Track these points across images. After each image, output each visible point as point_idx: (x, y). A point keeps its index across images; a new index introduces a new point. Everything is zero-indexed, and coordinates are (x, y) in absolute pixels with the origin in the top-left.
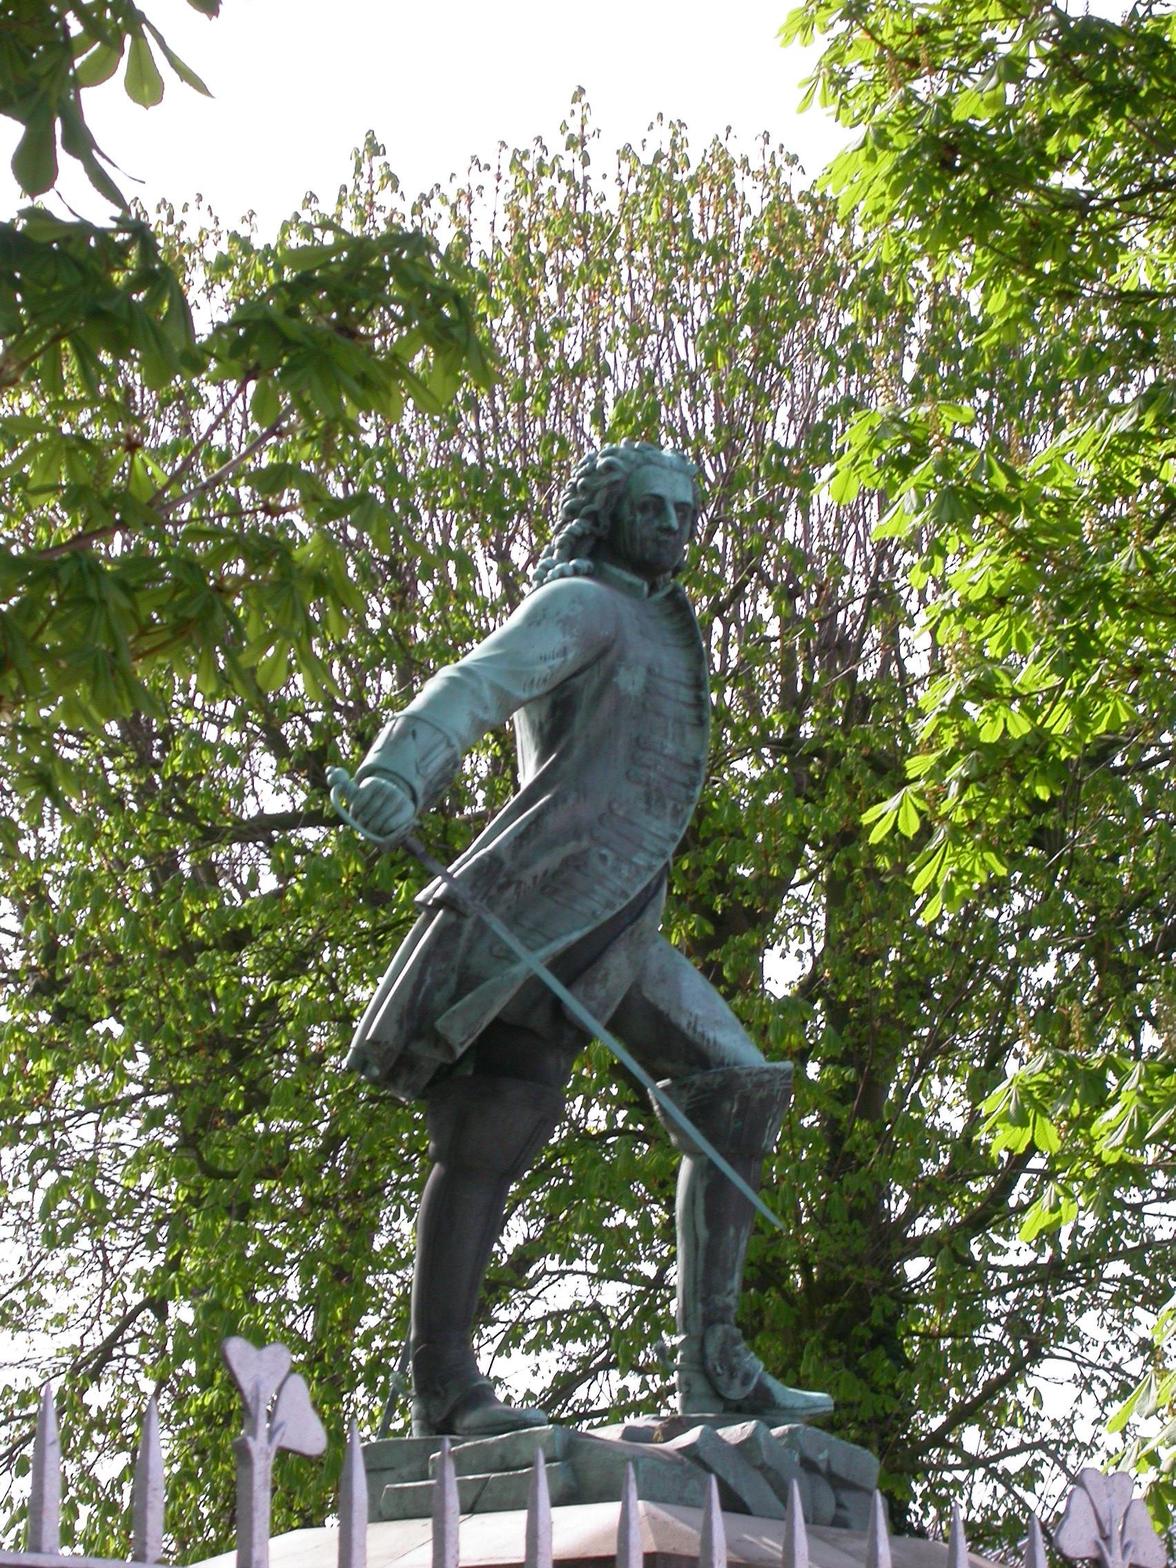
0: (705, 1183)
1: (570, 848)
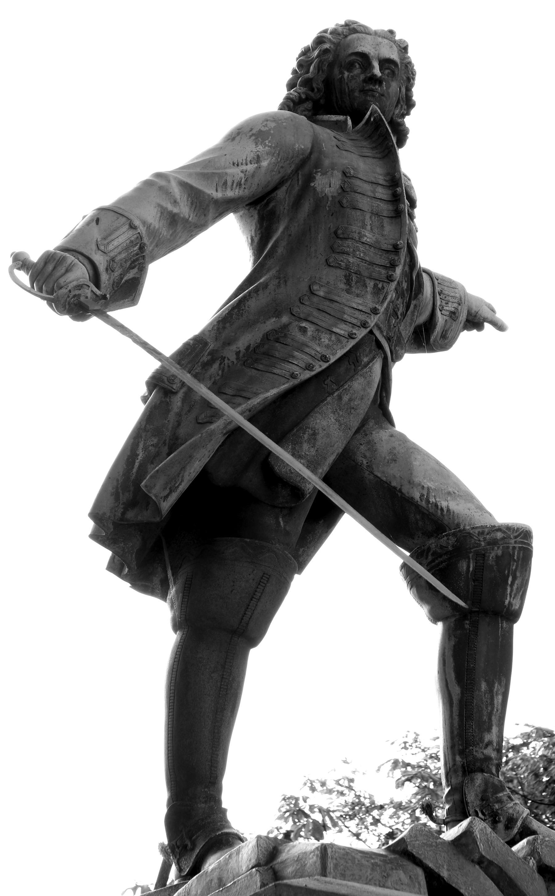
0: (453, 643)
1: (271, 324)
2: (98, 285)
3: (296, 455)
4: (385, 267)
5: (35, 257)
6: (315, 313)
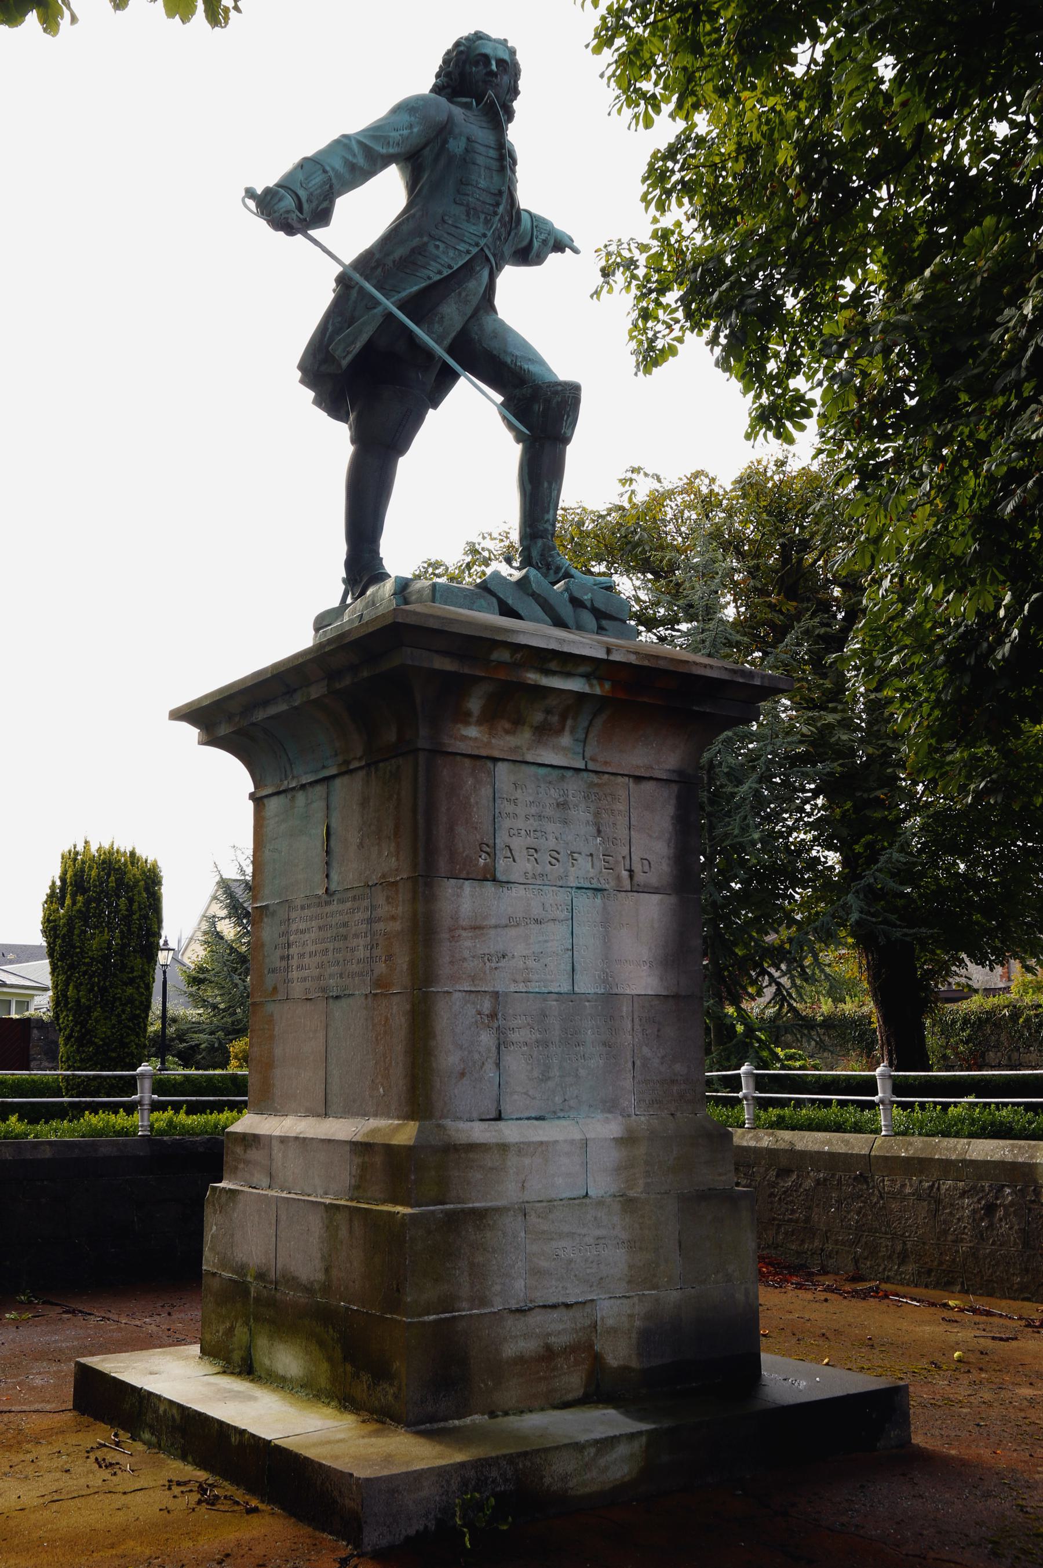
1: (416, 242)
2: (301, 213)
3: (429, 333)
4: (492, 205)
5: (259, 191)
6: (445, 235)
